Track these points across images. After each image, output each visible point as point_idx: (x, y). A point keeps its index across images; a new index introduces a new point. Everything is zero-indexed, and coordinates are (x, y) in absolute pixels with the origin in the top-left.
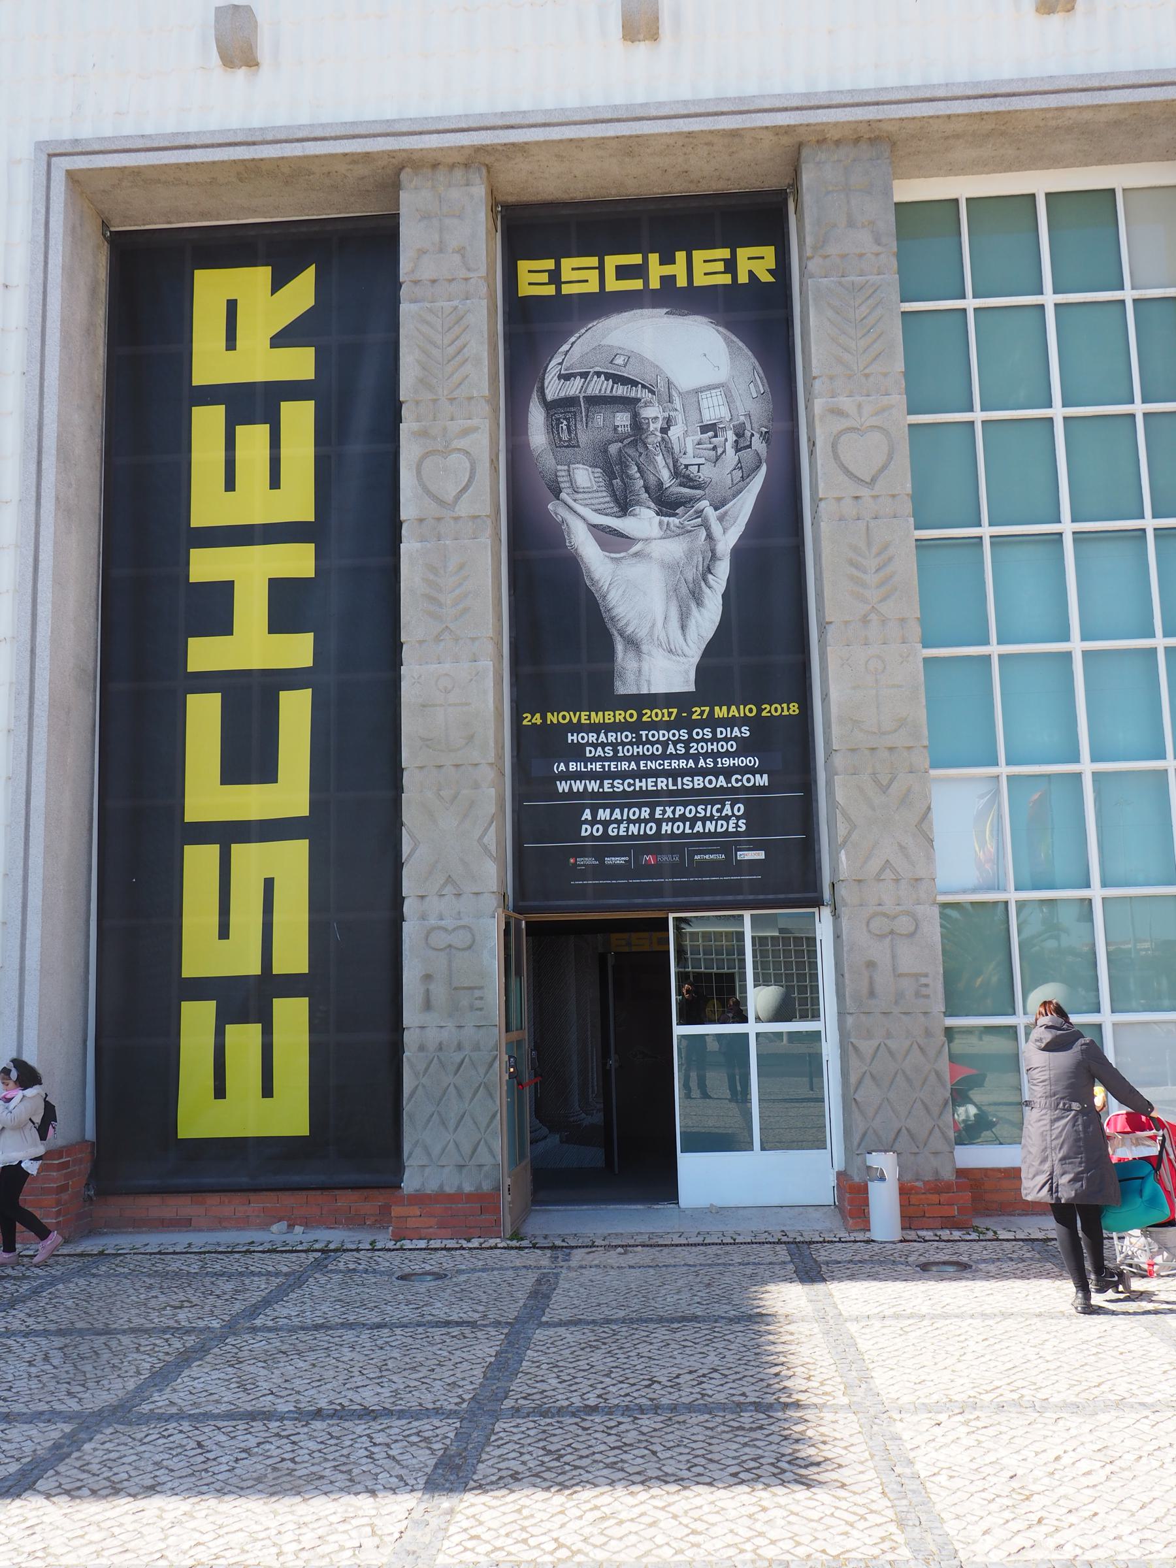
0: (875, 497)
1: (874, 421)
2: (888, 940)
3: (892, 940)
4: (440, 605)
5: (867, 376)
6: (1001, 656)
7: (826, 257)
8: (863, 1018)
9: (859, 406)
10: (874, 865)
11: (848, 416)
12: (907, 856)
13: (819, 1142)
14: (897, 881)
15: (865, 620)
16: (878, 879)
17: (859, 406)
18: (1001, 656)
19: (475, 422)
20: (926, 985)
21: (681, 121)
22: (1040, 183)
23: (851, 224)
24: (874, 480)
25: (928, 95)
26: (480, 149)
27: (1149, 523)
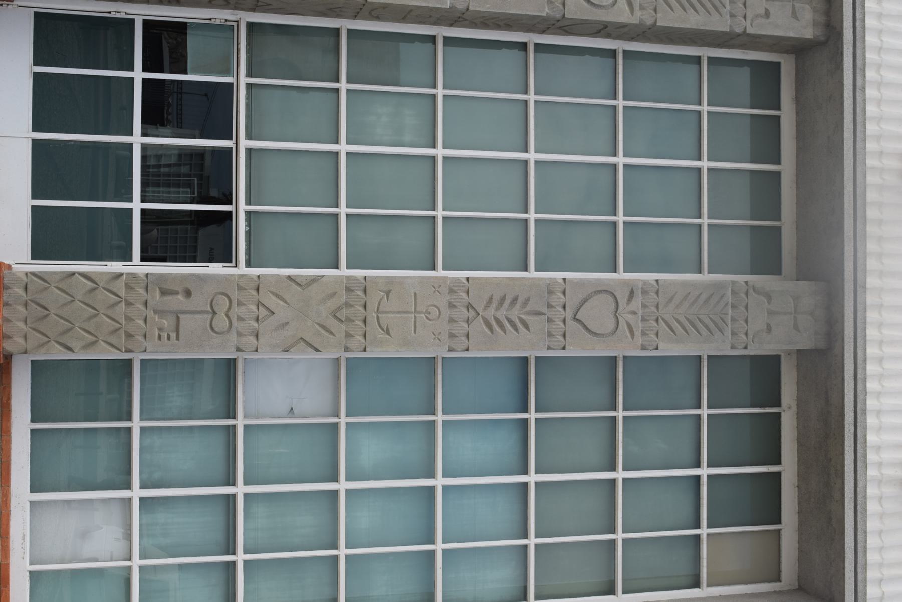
0: (564, 321)
1: (623, 325)
2: (209, 309)
3: (207, 312)
4: (497, 309)
5: (657, 320)
6: (444, 487)
7: (747, 294)
8: (143, 284)
9: (634, 313)
10: (272, 302)
11: (628, 304)
12: (277, 329)
13: (39, 252)
14: (257, 320)
15: (469, 306)
16: (259, 304)
17: (634, 313)
18: (444, 487)
19: (638, 13)
20: (169, 338)
21: (852, 189)
22: (788, 468)
23: (771, 313)
24: (579, 321)
25: (859, 376)
26: (840, 35)
27: (532, 541)
